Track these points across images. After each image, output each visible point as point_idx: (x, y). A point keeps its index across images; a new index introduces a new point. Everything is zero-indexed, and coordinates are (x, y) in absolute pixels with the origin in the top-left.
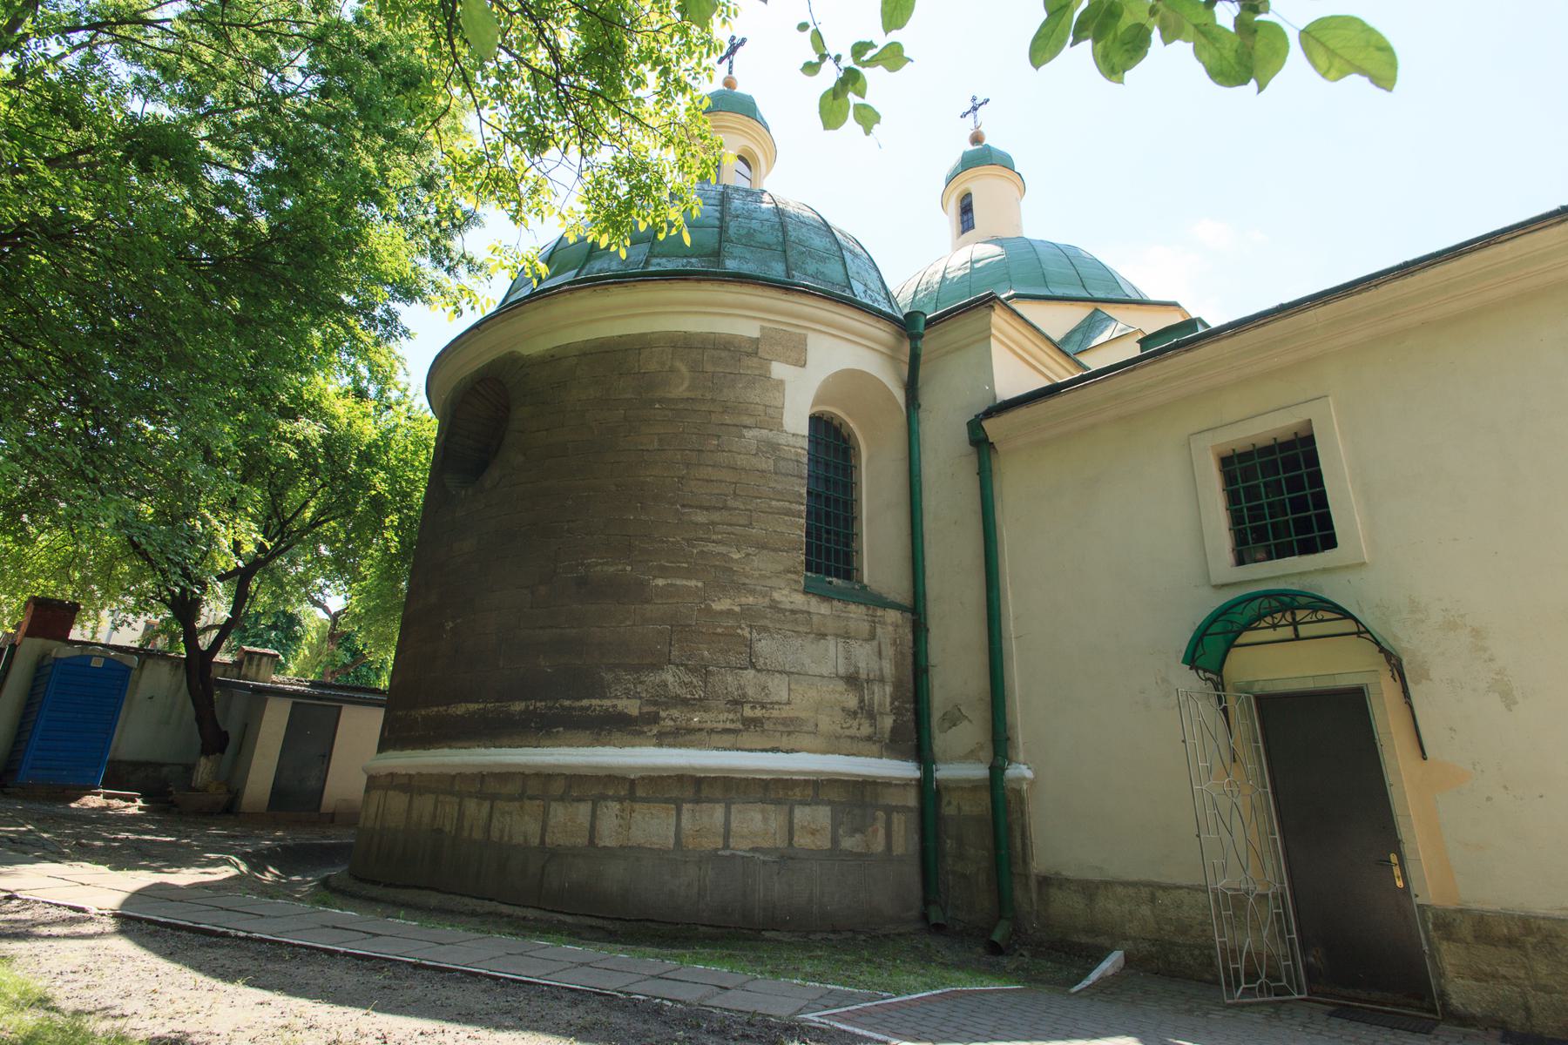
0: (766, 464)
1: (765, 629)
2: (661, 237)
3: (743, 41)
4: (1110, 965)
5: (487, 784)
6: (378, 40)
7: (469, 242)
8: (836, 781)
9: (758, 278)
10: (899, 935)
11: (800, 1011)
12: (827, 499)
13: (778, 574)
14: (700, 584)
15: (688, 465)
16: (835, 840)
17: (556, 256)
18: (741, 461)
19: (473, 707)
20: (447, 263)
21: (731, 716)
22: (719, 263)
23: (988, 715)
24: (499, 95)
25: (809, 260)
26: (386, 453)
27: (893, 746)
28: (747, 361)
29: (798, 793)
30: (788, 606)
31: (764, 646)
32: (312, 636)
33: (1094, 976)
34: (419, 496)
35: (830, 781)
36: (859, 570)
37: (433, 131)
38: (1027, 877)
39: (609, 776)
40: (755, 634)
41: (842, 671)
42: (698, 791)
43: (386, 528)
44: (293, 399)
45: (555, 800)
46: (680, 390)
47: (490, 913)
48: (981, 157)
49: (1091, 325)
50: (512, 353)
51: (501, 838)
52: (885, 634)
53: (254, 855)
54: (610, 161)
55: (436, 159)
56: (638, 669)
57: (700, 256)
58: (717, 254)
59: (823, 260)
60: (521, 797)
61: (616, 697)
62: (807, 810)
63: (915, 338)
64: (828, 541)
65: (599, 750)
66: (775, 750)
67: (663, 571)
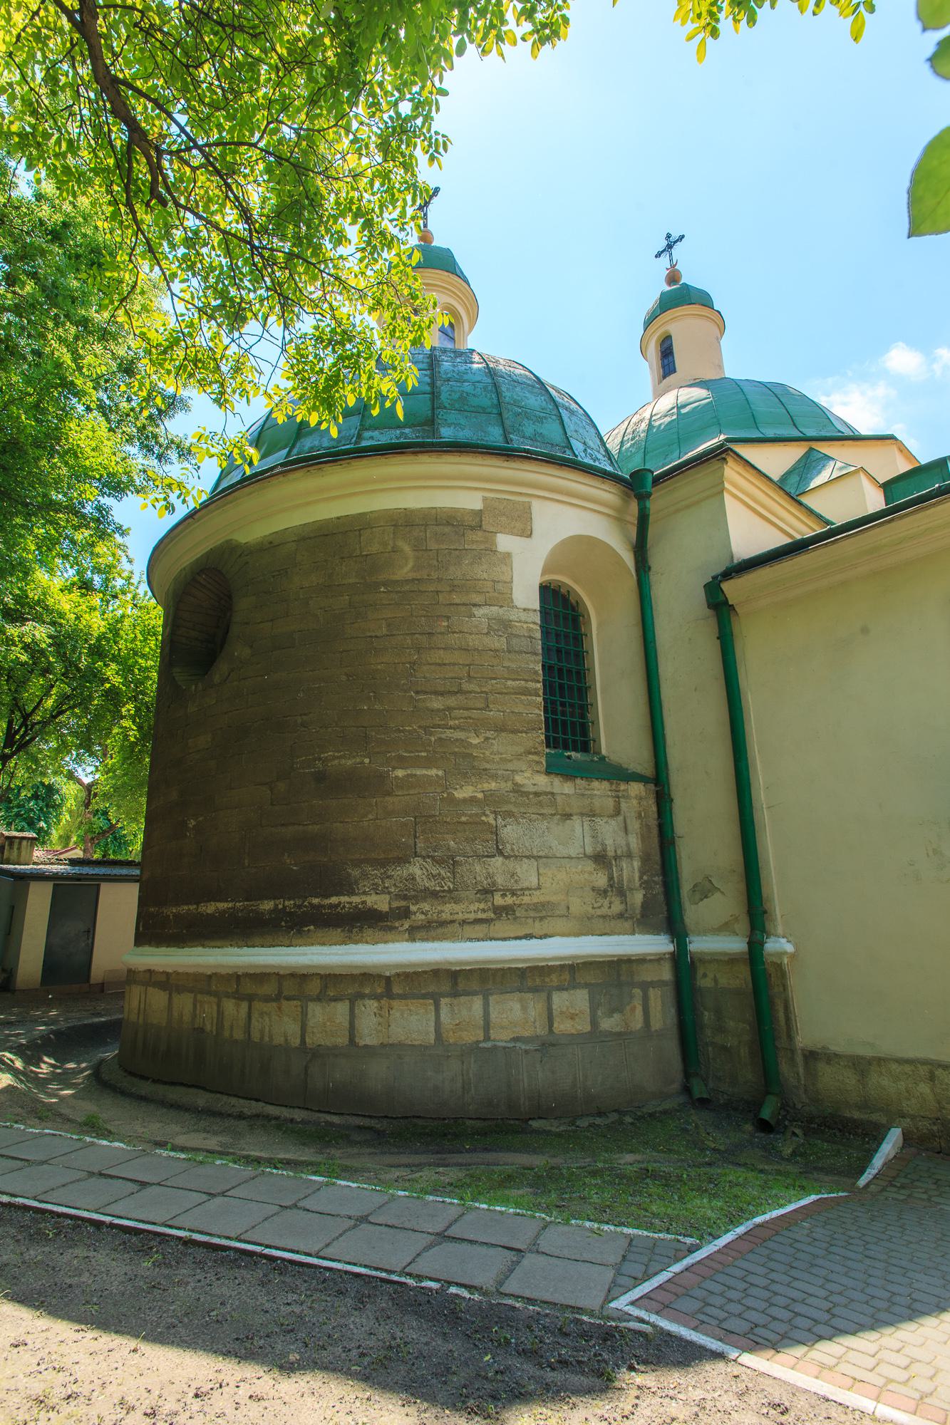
0: (499, 643)
1: (510, 814)
2: (375, 412)
3: (437, 190)
4: (890, 1145)
5: (244, 985)
6: (59, 218)
7: (177, 426)
8: (591, 963)
9: (477, 446)
10: (665, 1112)
11: (608, 1300)
12: (560, 670)
13: (519, 757)
14: (440, 773)
15: (419, 650)
16: (594, 1023)
17: (264, 436)
18: (473, 641)
19: (223, 906)
20: (156, 450)
21: (482, 906)
22: (435, 432)
23: (743, 886)
24: (189, 265)
25: (525, 422)
26: (116, 643)
27: (644, 921)
28: (471, 536)
29: (554, 979)
30: (532, 789)
31: (511, 832)
32: (71, 803)
33: (878, 1162)
34: (152, 686)
35: (584, 964)
36: (596, 741)
37: (121, 312)
38: (793, 1051)
39: (364, 974)
41: (589, 850)
42: (455, 984)
43: (122, 717)
44: (18, 600)
45: (313, 1000)
46: (405, 571)
47: (258, 1116)
48: (680, 297)
49: (808, 465)
50: (228, 542)
51: (262, 1038)
53: (27, 1047)
54: (310, 331)
55: (129, 346)
56: (383, 863)
57: (412, 426)
58: (431, 423)
59: (540, 420)
60: (278, 998)
61: (365, 893)
62: (565, 995)
63: (642, 498)
64: (563, 714)
65: (352, 948)
66: (529, 936)
67: (402, 762)
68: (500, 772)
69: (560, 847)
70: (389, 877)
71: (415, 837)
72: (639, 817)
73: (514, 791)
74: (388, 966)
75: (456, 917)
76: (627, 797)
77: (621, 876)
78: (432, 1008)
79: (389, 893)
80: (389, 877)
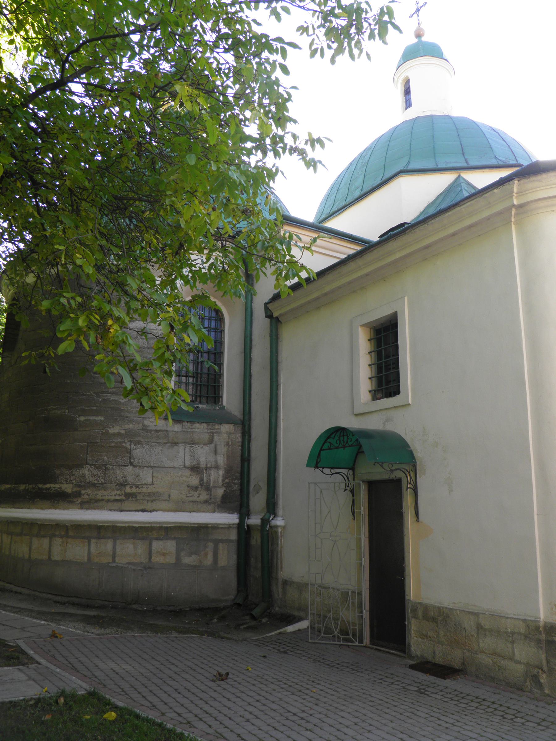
1: (139, 442)
8: (180, 527)
14: (102, 419)
16: (178, 558)
19: (8, 486)
21: (119, 492)
27: (225, 504)
29: (155, 534)
30: (154, 428)
31: (138, 452)
38: (277, 579)
40: (133, 446)
41: (188, 464)
52: (220, 440)
60: (21, 534)
61: (61, 483)
62: (161, 543)
66: (143, 511)
67: (84, 412)
68: (135, 419)
69: (169, 462)
70: (73, 475)
71: (87, 454)
72: (227, 444)
73: (143, 429)
74: (67, 521)
75: (104, 498)
76: (219, 433)
77: (209, 479)
78: (87, 544)
79: (72, 483)
80: (73, 475)
